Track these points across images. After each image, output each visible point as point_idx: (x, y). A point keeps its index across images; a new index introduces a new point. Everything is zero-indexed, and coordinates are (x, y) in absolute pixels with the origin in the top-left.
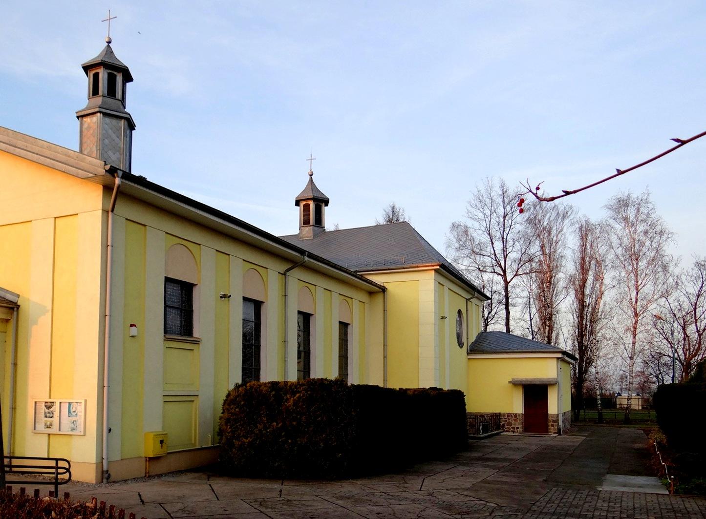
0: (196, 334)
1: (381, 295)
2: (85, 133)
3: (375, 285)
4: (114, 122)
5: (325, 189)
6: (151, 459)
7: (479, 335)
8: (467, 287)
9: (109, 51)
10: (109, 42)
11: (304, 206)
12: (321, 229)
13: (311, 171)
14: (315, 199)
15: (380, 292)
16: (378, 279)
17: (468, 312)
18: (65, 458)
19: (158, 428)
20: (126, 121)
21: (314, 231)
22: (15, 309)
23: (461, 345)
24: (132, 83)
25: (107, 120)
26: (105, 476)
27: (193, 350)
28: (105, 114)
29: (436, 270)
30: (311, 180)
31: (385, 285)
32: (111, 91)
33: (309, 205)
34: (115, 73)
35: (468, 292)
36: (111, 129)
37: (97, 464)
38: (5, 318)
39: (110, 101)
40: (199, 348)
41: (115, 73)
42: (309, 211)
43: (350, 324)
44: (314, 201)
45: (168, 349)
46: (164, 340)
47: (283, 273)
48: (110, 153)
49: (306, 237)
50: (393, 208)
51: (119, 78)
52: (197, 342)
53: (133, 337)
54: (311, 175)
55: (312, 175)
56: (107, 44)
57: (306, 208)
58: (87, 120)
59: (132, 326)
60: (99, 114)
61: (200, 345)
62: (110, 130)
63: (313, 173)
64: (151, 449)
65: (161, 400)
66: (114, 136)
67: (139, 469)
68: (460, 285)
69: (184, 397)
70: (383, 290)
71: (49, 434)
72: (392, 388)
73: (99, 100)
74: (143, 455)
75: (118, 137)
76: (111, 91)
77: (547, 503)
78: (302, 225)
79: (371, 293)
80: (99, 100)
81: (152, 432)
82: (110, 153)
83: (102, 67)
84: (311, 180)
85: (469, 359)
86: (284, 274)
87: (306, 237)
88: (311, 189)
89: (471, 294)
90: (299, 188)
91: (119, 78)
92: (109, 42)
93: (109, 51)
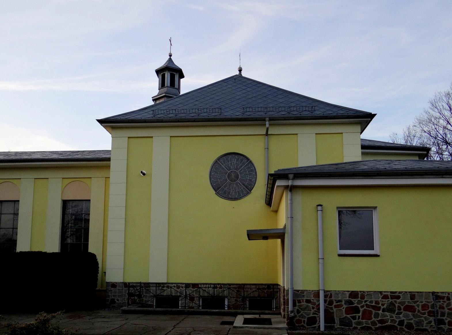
9: (170, 60)
34: (175, 73)
41: (175, 73)
56: (169, 57)
73: (165, 90)
80: (165, 90)
93: (170, 60)
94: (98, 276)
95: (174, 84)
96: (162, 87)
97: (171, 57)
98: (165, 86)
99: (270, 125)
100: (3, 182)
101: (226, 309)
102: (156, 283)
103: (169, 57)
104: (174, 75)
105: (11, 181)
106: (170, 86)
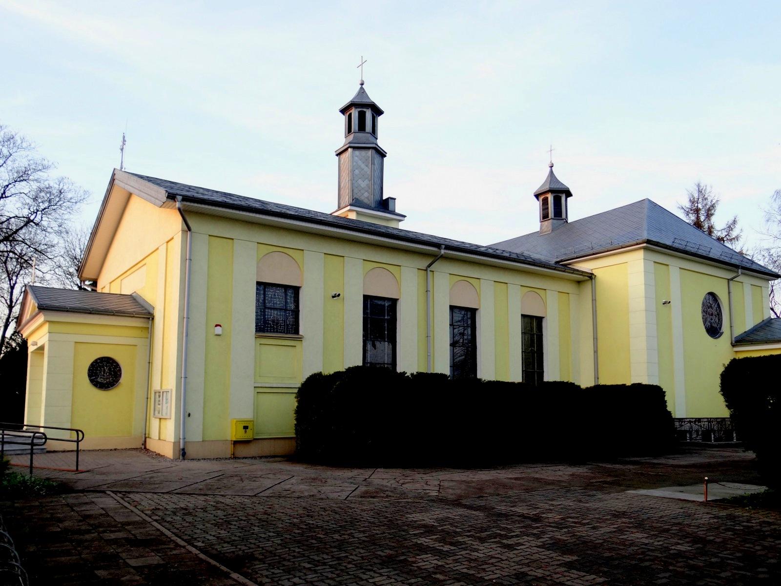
0: (301, 333)
1: (590, 281)
2: (342, 166)
3: (582, 273)
4: (363, 153)
5: (565, 179)
6: (236, 443)
7: (763, 323)
8: (724, 266)
9: (362, 91)
10: (362, 84)
11: (543, 200)
12: (562, 222)
13: (551, 162)
14: (551, 191)
15: (587, 280)
16: (585, 266)
17: (732, 294)
18: (85, 436)
19: (247, 415)
20: (373, 150)
21: (553, 224)
22: (151, 319)
23: (714, 331)
24: (383, 115)
25: (357, 152)
26: (183, 454)
27: (295, 346)
28: (354, 148)
29: (645, 248)
30: (552, 172)
31: (594, 272)
32: (362, 127)
33: (547, 198)
34: (365, 110)
35: (730, 270)
36: (360, 160)
37: (174, 443)
38: (145, 326)
39: (361, 135)
40: (302, 343)
41: (365, 110)
42: (548, 204)
43: (544, 317)
44: (551, 193)
45: (262, 346)
46: (256, 338)
47: (425, 269)
48: (360, 181)
49: (545, 232)
50: (699, 186)
51: (369, 114)
52: (300, 339)
53: (217, 335)
54: (552, 167)
55: (552, 167)
56: (360, 86)
57: (545, 202)
58: (344, 156)
59: (217, 326)
60: (350, 149)
61: (303, 342)
62: (360, 161)
63: (553, 164)
64: (234, 433)
65: (251, 392)
66: (363, 166)
67: (228, 450)
68: (701, 261)
69: (265, 389)
70: (591, 276)
71: (160, 419)
72: (651, 384)
73: (351, 137)
74: (229, 438)
75: (367, 166)
76: (362, 127)
77: (68, 505)
78: (542, 220)
79: (579, 282)
80: (351, 137)
81: (236, 419)
82: (360, 181)
83: (353, 107)
84: (552, 172)
85: (736, 352)
86: (426, 270)
87: (545, 232)
88: (549, 182)
89: (736, 272)
90: (539, 181)
91: (369, 114)
92: (362, 84)
93: (362, 91)
94: (670, 413)
95: (559, 212)
96: (348, 133)
97: (363, 86)
98: (548, 217)
99: (742, 273)
100: (283, 252)
101: (713, 441)
102: (296, 312)
103: (360, 86)
104: (560, 198)
105: (290, 252)
106: (359, 130)
